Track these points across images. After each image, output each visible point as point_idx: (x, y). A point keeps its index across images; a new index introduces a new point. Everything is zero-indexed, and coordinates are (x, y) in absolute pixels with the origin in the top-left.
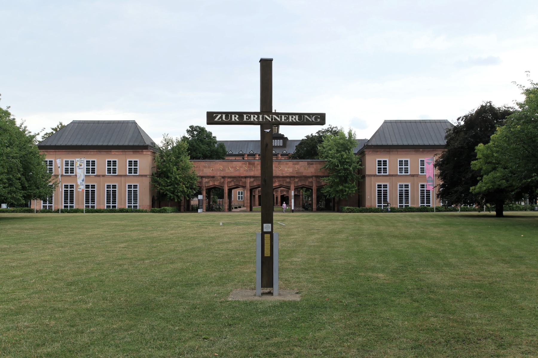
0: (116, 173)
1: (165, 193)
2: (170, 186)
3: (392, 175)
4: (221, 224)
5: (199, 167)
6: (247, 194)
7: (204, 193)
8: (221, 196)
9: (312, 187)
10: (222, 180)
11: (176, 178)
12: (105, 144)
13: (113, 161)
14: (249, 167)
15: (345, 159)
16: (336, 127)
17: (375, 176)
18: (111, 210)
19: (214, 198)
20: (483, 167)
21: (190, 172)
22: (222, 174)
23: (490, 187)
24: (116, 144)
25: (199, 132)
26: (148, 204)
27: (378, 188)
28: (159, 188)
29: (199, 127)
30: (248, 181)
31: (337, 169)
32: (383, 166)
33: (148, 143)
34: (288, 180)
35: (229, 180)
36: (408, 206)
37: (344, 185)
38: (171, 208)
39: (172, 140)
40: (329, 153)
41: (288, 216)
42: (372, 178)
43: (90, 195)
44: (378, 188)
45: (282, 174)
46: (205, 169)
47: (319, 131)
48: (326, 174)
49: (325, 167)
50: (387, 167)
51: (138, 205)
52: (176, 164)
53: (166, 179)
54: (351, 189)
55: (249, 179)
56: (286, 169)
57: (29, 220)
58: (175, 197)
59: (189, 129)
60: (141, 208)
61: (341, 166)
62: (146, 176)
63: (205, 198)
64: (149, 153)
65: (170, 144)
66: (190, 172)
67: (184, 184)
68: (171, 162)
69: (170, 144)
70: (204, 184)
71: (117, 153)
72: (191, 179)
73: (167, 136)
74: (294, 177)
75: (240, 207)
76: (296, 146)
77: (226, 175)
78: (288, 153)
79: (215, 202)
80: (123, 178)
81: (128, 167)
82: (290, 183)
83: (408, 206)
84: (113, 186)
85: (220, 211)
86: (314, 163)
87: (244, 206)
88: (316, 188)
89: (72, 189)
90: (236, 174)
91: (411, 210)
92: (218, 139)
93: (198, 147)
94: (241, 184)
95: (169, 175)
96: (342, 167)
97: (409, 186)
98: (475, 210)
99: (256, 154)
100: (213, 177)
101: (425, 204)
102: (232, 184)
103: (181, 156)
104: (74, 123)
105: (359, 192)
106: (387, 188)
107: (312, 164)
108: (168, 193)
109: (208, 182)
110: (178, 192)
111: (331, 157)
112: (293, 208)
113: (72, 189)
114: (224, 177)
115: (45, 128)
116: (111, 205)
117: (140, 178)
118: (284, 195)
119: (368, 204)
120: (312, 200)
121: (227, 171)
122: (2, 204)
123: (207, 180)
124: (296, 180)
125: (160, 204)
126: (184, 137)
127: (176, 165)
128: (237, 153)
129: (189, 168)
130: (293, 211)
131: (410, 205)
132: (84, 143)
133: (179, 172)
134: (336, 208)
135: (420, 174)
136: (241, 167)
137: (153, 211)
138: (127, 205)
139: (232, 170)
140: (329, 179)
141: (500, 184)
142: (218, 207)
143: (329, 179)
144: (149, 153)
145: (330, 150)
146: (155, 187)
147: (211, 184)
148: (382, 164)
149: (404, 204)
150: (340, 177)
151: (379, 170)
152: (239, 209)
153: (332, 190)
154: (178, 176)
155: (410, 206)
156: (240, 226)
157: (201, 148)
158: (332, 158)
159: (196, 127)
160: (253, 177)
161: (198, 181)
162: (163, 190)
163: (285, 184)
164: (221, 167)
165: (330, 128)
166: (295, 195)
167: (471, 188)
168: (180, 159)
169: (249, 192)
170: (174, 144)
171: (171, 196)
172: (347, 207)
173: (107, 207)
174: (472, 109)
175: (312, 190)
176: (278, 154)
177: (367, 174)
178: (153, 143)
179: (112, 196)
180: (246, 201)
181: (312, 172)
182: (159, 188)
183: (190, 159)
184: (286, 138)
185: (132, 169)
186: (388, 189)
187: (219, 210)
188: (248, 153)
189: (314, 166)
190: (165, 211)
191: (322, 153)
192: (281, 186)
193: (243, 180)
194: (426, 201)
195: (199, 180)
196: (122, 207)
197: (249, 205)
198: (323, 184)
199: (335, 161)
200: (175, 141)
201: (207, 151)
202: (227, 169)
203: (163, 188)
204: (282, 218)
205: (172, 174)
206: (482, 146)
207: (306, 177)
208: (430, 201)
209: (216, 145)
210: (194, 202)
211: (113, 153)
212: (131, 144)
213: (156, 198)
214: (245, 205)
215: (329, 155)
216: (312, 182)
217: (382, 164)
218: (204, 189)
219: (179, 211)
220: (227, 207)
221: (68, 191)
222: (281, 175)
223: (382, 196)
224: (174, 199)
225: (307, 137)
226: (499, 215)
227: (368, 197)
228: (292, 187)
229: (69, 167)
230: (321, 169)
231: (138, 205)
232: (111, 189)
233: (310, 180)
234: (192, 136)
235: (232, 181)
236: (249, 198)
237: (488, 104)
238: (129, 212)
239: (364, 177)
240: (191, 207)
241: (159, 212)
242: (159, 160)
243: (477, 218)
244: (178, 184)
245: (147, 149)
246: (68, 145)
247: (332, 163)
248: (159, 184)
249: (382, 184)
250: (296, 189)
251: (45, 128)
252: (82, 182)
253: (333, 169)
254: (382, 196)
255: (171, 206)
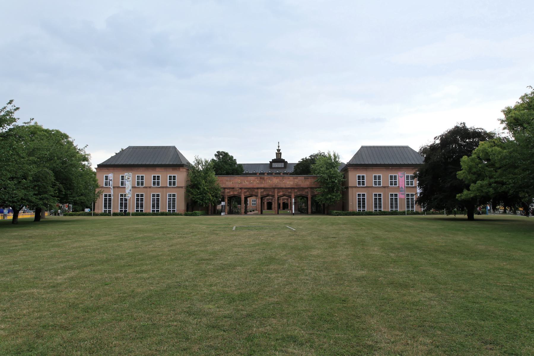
0: (159, 185)
1: (196, 200)
2: (200, 195)
3: (369, 187)
4: (234, 228)
5: (223, 181)
6: (259, 201)
7: (226, 200)
8: (240, 203)
9: (308, 196)
10: (240, 190)
11: (204, 189)
12: (152, 163)
13: (173, 176)
14: (260, 181)
15: (333, 174)
16: (324, 153)
17: (356, 187)
18: (139, 213)
19: (235, 204)
20: (468, 176)
21: (215, 185)
22: (240, 187)
23: (478, 194)
24: (160, 163)
25: (224, 156)
26: (184, 209)
27: (358, 196)
28: (191, 196)
29: (224, 152)
30: (260, 191)
31: (327, 182)
32: (362, 180)
33: (185, 163)
34: (290, 191)
35: (245, 190)
36: (381, 210)
37: (332, 194)
38: (201, 212)
39: (201, 161)
40: (321, 170)
41: (293, 219)
42: (354, 189)
43: (140, 201)
44: (358, 196)
45: (285, 186)
46: (227, 182)
47: (311, 155)
48: (318, 186)
49: (317, 181)
50: (365, 180)
51: (176, 209)
52: (205, 178)
53: (197, 190)
54: (337, 197)
55: (260, 190)
56: (288, 182)
57: (70, 223)
58: (204, 203)
59: (217, 153)
60: (178, 212)
61: (330, 180)
62: (182, 187)
63: (227, 204)
64: (185, 170)
65: (200, 163)
66: (215, 185)
67: (211, 194)
68: (201, 177)
69: (200, 163)
70: (226, 193)
71: (160, 170)
72: (216, 190)
73: (198, 157)
74: (294, 188)
75: (253, 211)
76: (294, 166)
77: (243, 187)
78: (288, 172)
79: (236, 207)
80: (164, 189)
81: (168, 181)
82: (291, 192)
83: (381, 210)
84: (157, 195)
85: (238, 214)
86: (309, 177)
87: (256, 210)
88: (311, 197)
89: (142, 197)
90: (250, 186)
91: (385, 213)
92: (238, 162)
93: (222, 166)
94: (254, 194)
95: (200, 187)
96: (330, 181)
97: (382, 195)
98: (433, 213)
99: (265, 173)
100: (233, 188)
101: (394, 209)
102: (248, 193)
103: (208, 173)
104: (129, 148)
105: (343, 200)
106: (365, 196)
107: (308, 179)
108: (198, 200)
109: (229, 192)
110: (205, 200)
111: (322, 173)
112: (293, 212)
113: (142, 197)
114: (241, 188)
115: (88, 145)
116: (156, 209)
117: (178, 189)
118: (284, 202)
119: (350, 209)
120: (307, 205)
121: (244, 183)
122: (85, 209)
123: (228, 191)
124: (296, 191)
125: (193, 209)
126: (213, 160)
127: (204, 179)
128: (252, 172)
129: (215, 181)
130: (293, 214)
131: (382, 209)
132: (136, 162)
133: (207, 184)
134: (326, 212)
135: (390, 186)
136: (254, 181)
137: (186, 215)
138: (168, 209)
139: (247, 183)
140: (321, 190)
141: (487, 191)
142: (237, 211)
143: (321, 190)
144: (185, 170)
145: (322, 167)
146: (189, 196)
147: (231, 193)
148: (361, 178)
149: (378, 209)
150: (329, 188)
151: (359, 183)
152: (253, 213)
153: (323, 198)
154: (205, 188)
155: (382, 210)
156: (251, 232)
157: (225, 167)
158: (323, 174)
159: (222, 152)
160: (264, 188)
161: (222, 191)
162: (195, 198)
163: (287, 194)
164: (239, 181)
165: (320, 153)
166: (295, 202)
167: (458, 196)
168: (208, 174)
169: (260, 200)
170: (203, 163)
171: (200, 203)
172: (335, 211)
173: (137, 211)
174: (446, 130)
175: (307, 198)
176: (281, 173)
177: (350, 185)
178: (189, 163)
179: (157, 203)
180: (257, 207)
181: (307, 185)
182: (191, 196)
183: (215, 175)
184: (286, 162)
185: (171, 182)
186: (365, 197)
187: (238, 213)
188: (259, 172)
189: (309, 180)
190: (195, 215)
191: (315, 170)
192: (284, 195)
193: (256, 190)
194: (362, 206)
195: (222, 190)
196: (164, 211)
197: (260, 209)
198: (316, 193)
199: (325, 176)
200: (204, 161)
201: (229, 169)
202: (243, 182)
203: (195, 197)
204: (289, 221)
205: (201, 186)
206: (466, 158)
207: (303, 189)
208: (365, 206)
209: (236, 166)
210: (219, 207)
211: (157, 170)
212: (171, 163)
213: (190, 204)
214: (257, 209)
215: (321, 171)
216: (307, 192)
217: (361, 178)
218: (226, 197)
219: (207, 214)
220: (243, 211)
221: (139, 199)
222: (284, 187)
223: (362, 202)
224: (203, 205)
225: (303, 159)
226: (471, 218)
227: (350, 203)
228: (293, 196)
229: (140, 181)
230: (314, 182)
231: (176, 209)
232: (156, 197)
233: (306, 190)
234: (219, 159)
235: (248, 191)
236: (260, 204)
237: (463, 125)
238: (168, 215)
239: (347, 188)
240: (216, 211)
241: (191, 215)
242: (192, 175)
243: (452, 222)
244: (206, 194)
245: (183, 167)
246: (123, 164)
247: (323, 177)
248: (192, 194)
249: (361, 193)
250: (296, 198)
251: (88, 145)
252: (129, 191)
253: (323, 182)
254: (362, 202)
255: (201, 211)
